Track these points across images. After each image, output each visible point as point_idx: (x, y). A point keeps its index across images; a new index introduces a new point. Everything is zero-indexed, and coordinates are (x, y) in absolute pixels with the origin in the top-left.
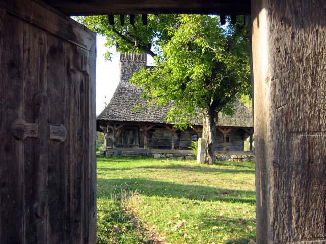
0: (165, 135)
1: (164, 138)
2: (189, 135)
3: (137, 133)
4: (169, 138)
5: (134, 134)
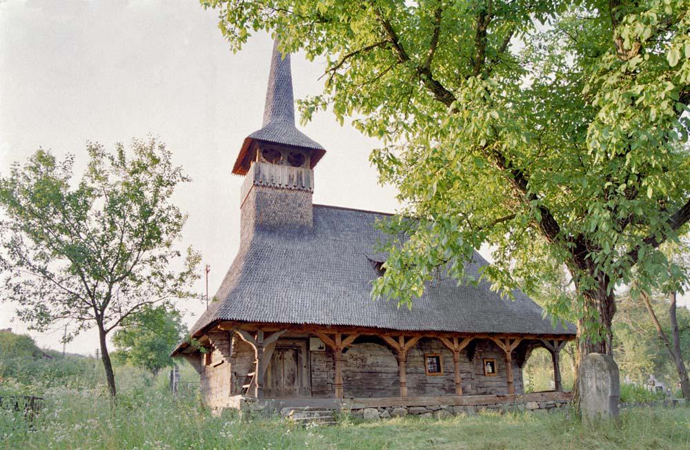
0: (370, 361)
1: (367, 369)
2: (422, 359)
3: (303, 356)
4: (378, 369)
5: (296, 358)
